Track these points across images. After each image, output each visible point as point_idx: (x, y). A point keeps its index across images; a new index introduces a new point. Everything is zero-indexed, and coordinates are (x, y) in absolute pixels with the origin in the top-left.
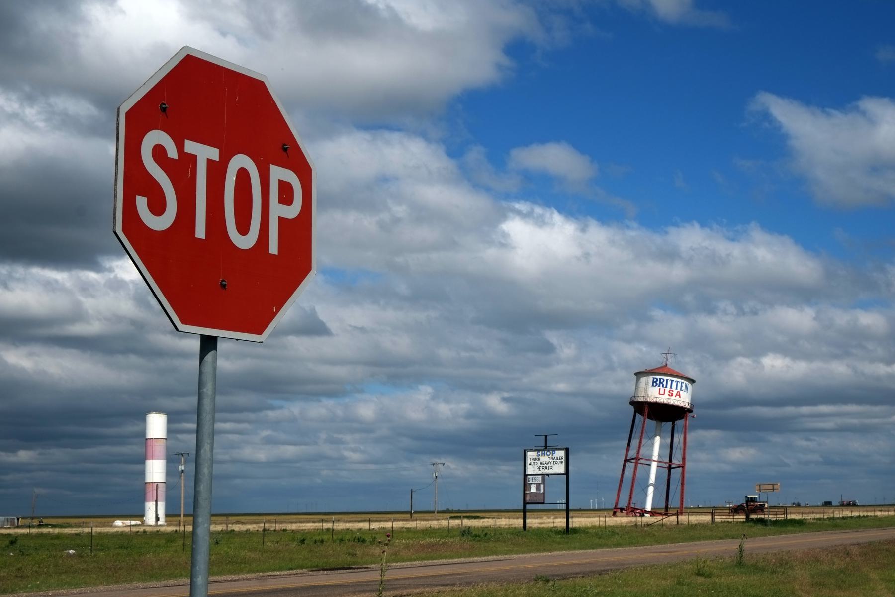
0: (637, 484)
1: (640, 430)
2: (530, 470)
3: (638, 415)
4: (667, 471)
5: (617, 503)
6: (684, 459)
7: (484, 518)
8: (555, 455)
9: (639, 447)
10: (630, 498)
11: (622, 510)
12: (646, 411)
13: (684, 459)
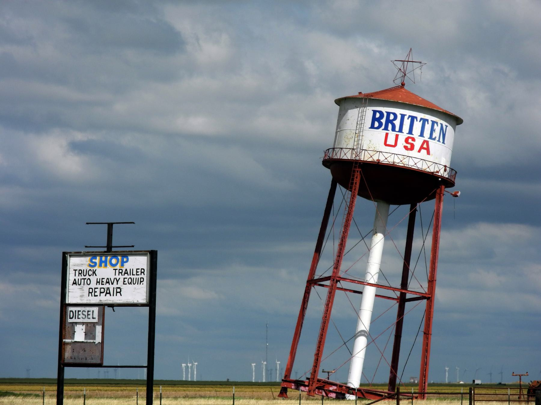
0: (332, 333)
2: (75, 295)
3: (340, 189)
4: (395, 305)
5: (289, 370)
6: (432, 282)
8: (127, 266)
9: (340, 255)
11: (298, 384)
12: (357, 180)
13: (432, 282)
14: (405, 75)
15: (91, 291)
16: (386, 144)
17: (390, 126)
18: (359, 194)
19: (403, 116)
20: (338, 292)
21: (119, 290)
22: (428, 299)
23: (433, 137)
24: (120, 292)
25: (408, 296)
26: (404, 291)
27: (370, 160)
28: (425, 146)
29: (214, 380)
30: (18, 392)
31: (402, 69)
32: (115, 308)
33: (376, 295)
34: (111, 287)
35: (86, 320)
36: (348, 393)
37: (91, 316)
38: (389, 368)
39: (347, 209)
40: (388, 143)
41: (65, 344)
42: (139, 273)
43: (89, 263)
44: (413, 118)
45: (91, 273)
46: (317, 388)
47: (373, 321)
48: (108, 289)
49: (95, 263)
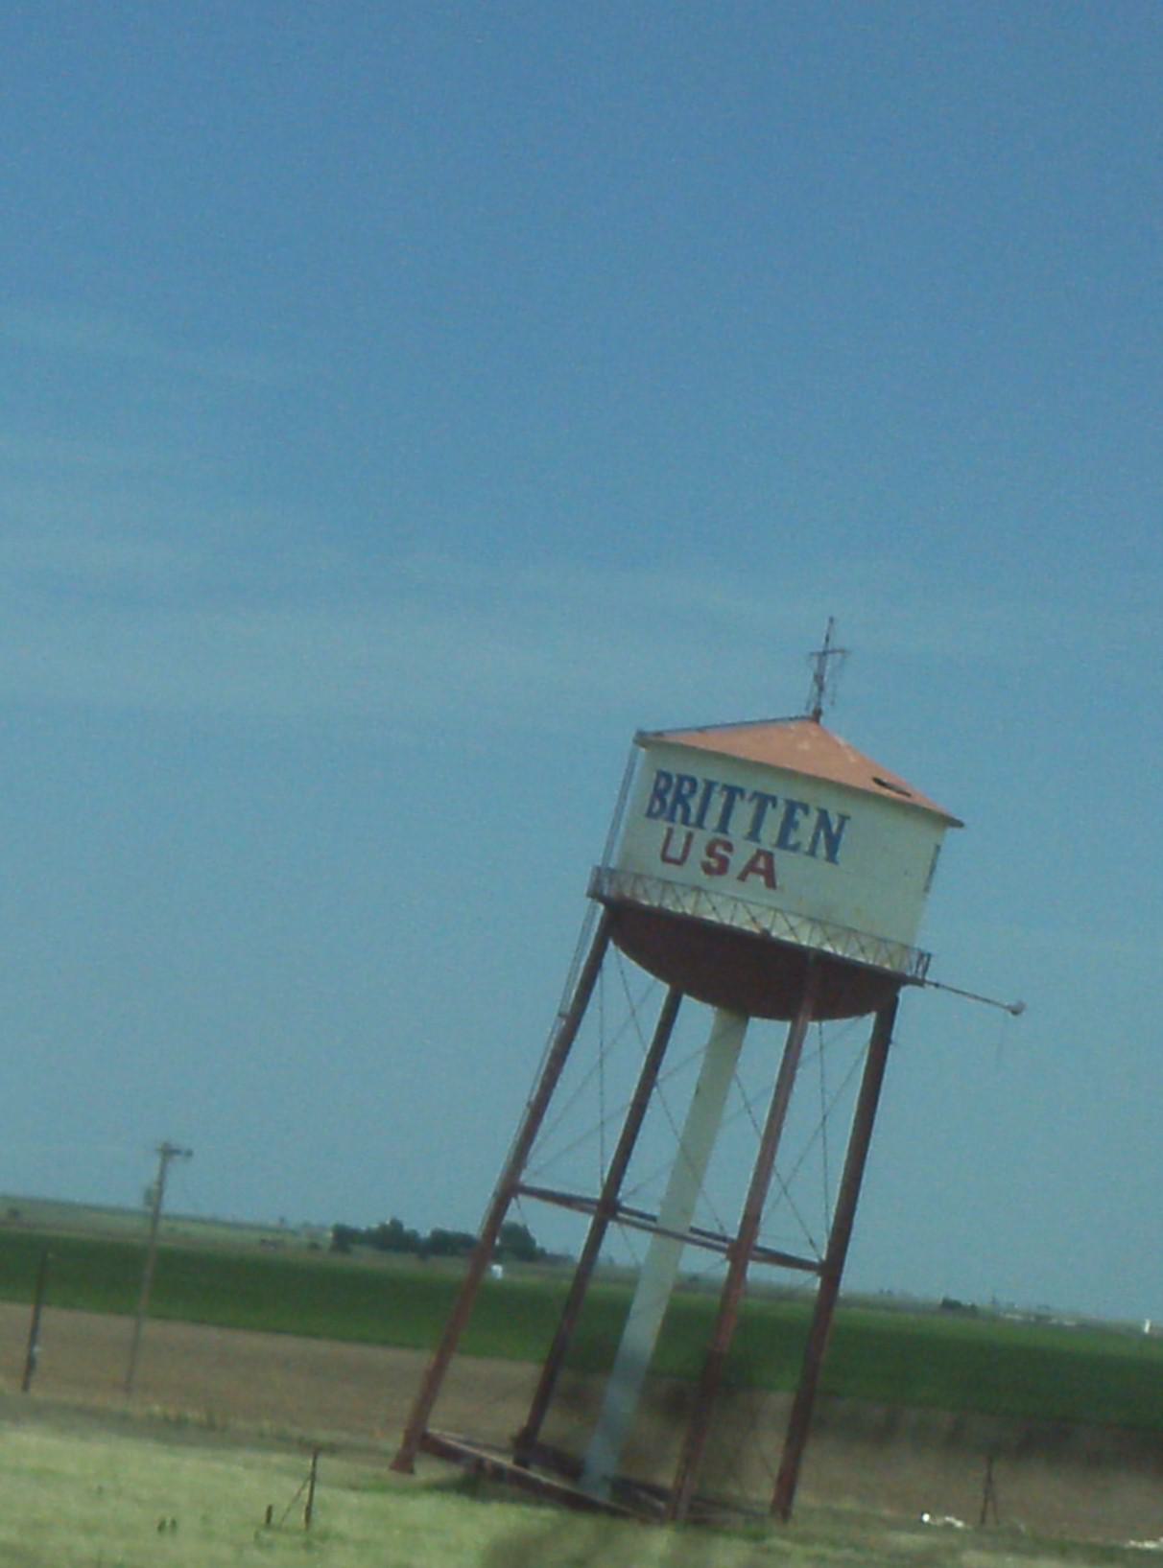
23: (792, 842)
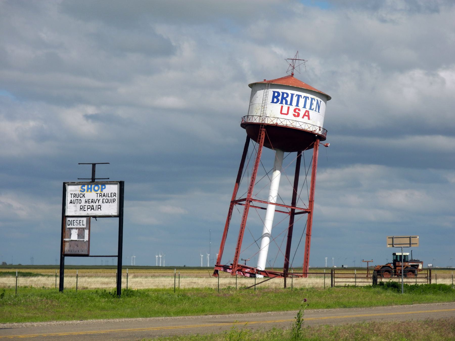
0: (246, 235)
1: (253, 163)
2: (71, 210)
3: (252, 142)
4: (288, 217)
5: (219, 259)
6: (311, 202)
7: (36, 275)
8: (105, 191)
10: (237, 253)
11: (226, 268)
12: (263, 136)
13: (311, 202)
14: (294, 68)
15: (81, 207)
16: (281, 113)
17: (284, 101)
18: (264, 145)
19: (292, 95)
20: (250, 208)
21: (99, 207)
22: (309, 212)
24: (100, 208)
25: (296, 211)
26: (293, 208)
27: (271, 123)
28: (307, 114)
29: (190, 266)
30: (45, 274)
31: (292, 64)
32: (97, 218)
33: (275, 211)
34: (95, 205)
35: (79, 226)
36: (258, 273)
37: (81, 224)
38: (284, 258)
39: (257, 155)
40: (283, 112)
41: (65, 242)
42: (113, 196)
43: (80, 189)
44: (299, 96)
45: (81, 196)
46: (238, 270)
47: (273, 227)
48: (93, 206)
49: (84, 190)
